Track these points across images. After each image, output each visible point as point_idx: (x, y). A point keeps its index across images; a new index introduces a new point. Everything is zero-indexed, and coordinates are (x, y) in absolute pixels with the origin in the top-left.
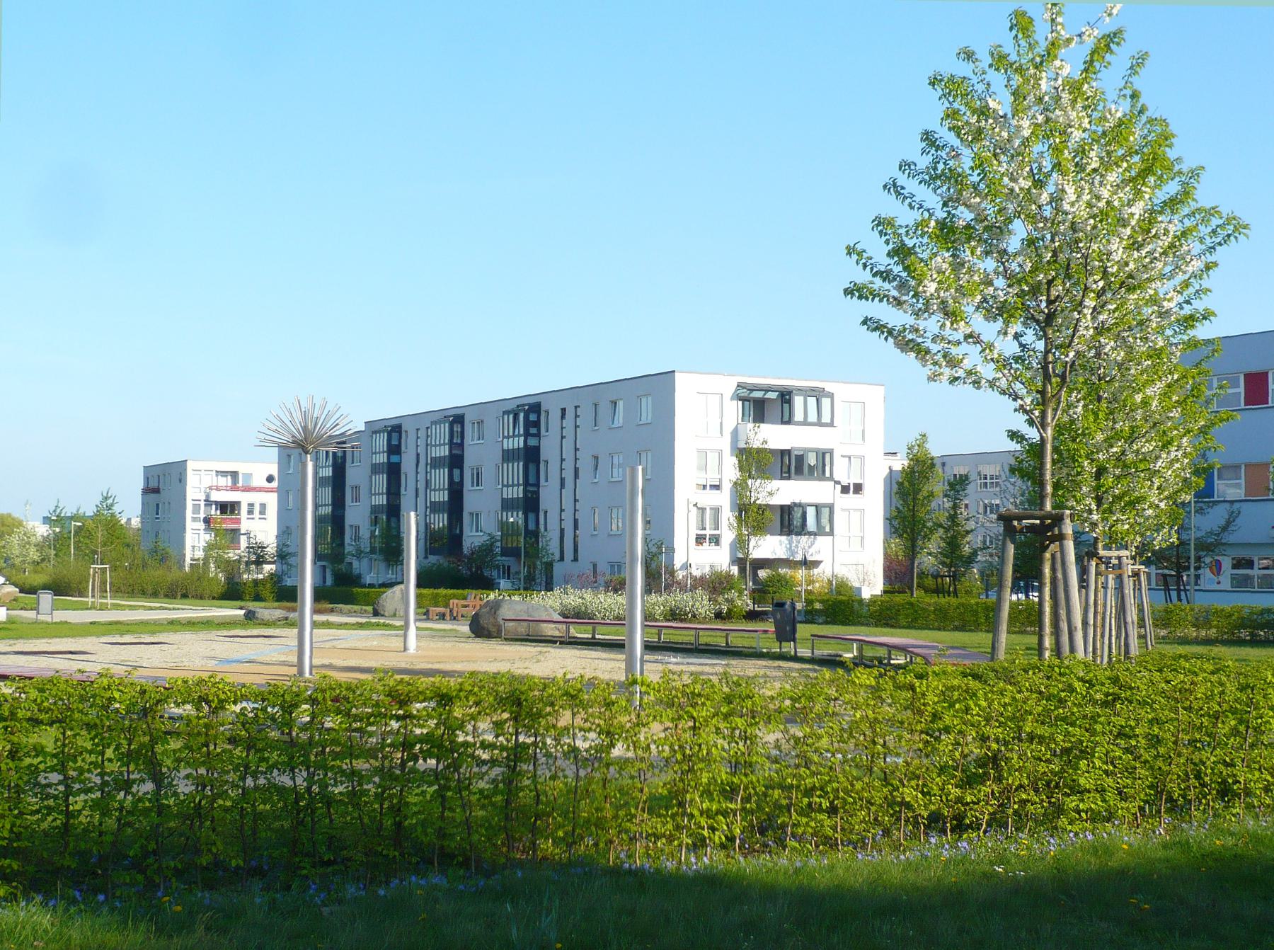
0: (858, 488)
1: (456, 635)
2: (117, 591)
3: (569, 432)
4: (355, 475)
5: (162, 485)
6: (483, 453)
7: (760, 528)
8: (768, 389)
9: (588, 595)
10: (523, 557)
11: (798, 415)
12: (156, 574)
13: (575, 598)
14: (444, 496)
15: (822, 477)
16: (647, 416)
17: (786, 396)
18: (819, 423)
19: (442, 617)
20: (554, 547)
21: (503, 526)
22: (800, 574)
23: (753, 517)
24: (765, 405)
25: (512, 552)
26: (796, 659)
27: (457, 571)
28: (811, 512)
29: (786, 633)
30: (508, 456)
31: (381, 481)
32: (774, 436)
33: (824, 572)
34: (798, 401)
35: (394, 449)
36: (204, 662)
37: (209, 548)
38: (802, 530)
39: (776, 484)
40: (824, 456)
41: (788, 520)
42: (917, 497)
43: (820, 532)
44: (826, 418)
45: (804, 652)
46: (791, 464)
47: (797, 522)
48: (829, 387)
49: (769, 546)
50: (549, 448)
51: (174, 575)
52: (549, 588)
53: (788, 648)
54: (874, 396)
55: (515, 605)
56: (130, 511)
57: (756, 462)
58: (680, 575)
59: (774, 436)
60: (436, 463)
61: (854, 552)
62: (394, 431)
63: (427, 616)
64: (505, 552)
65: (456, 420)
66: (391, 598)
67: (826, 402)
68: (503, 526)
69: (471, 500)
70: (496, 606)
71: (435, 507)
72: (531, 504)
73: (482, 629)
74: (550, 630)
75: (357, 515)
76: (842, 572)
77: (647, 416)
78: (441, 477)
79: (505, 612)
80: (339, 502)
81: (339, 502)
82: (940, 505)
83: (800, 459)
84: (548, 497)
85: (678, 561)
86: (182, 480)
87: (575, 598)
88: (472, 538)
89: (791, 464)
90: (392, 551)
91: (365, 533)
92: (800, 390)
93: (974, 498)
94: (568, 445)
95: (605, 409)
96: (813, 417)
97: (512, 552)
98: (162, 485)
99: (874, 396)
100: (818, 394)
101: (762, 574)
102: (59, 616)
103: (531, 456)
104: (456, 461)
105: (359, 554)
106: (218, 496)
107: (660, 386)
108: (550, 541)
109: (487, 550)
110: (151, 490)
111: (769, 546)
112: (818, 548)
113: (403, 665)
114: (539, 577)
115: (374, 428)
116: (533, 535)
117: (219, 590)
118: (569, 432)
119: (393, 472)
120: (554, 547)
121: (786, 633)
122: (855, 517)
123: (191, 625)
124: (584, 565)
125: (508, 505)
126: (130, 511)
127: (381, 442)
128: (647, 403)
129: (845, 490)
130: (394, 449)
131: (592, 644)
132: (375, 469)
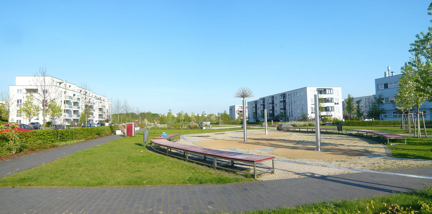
0: (338, 104)
1: (274, 130)
2: (224, 123)
3: (290, 98)
4: (258, 106)
5: (232, 109)
6: (277, 102)
7: (322, 111)
8: (322, 89)
9: (295, 122)
10: (284, 117)
11: (327, 93)
12: (231, 121)
13: (293, 123)
14: (271, 108)
15: (332, 102)
16: (302, 94)
17: (325, 90)
18: (331, 94)
19: (272, 126)
20: (289, 115)
21: (281, 112)
22: (329, 117)
23: (321, 109)
24: (322, 91)
25: (282, 116)
26: (342, 134)
27: (274, 118)
28: (330, 108)
29: (340, 129)
30: (281, 102)
31: (262, 106)
32: (324, 96)
33: (333, 117)
34: (327, 90)
35: (264, 102)
36: (228, 138)
37: (239, 117)
38: (329, 111)
39: (324, 104)
40: (332, 99)
41: (327, 109)
42: (348, 104)
43: (332, 111)
44: (332, 93)
45: (344, 132)
46: (326, 100)
47: (328, 109)
48: (332, 88)
49: (324, 113)
50: (287, 100)
51: (234, 121)
52: (288, 121)
53: (341, 132)
54: (340, 89)
55: (285, 125)
56: (228, 113)
57: (321, 100)
58: (309, 118)
59: (324, 96)
60: (270, 103)
61: (338, 114)
62: (264, 99)
63: (270, 126)
64: (281, 116)
65: (273, 97)
66: (264, 124)
67: (332, 90)
68: (281, 112)
69: (275, 109)
70: (281, 125)
71: (270, 110)
72: (285, 109)
73: (279, 129)
74: (291, 129)
75: (259, 112)
76: (336, 117)
77: (302, 94)
78: (271, 105)
79: (283, 126)
80: (256, 110)
81: (256, 110)
82: (355, 105)
83: (328, 100)
84: (287, 108)
85: (309, 116)
86: (235, 108)
87: (293, 123)
88: (276, 114)
89: (326, 100)
90: (263, 116)
91: (260, 114)
92: (327, 89)
93: (362, 104)
94: (290, 99)
95: (295, 94)
96: (330, 93)
97: (282, 116)
98: (232, 109)
99: (340, 89)
100: (330, 89)
101: (323, 118)
102: (213, 128)
103: (284, 102)
104: (273, 103)
105: (259, 117)
106: (239, 110)
107: (304, 89)
108: (288, 114)
109: (278, 116)
110: (231, 110)
111: (324, 113)
112: (332, 113)
113: (265, 138)
114: (287, 120)
115: (260, 99)
116: (285, 113)
117: (240, 123)
118: (290, 98)
119: (264, 105)
120: (289, 115)
121: (340, 129)
122: (338, 108)
123: (231, 129)
124: (293, 117)
125: (281, 109)
126: (228, 113)
127: (262, 101)
128: (302, 92)
129: (336, 104)
130: (264, 102)
131: (300, 132)
132: (261, 105)
